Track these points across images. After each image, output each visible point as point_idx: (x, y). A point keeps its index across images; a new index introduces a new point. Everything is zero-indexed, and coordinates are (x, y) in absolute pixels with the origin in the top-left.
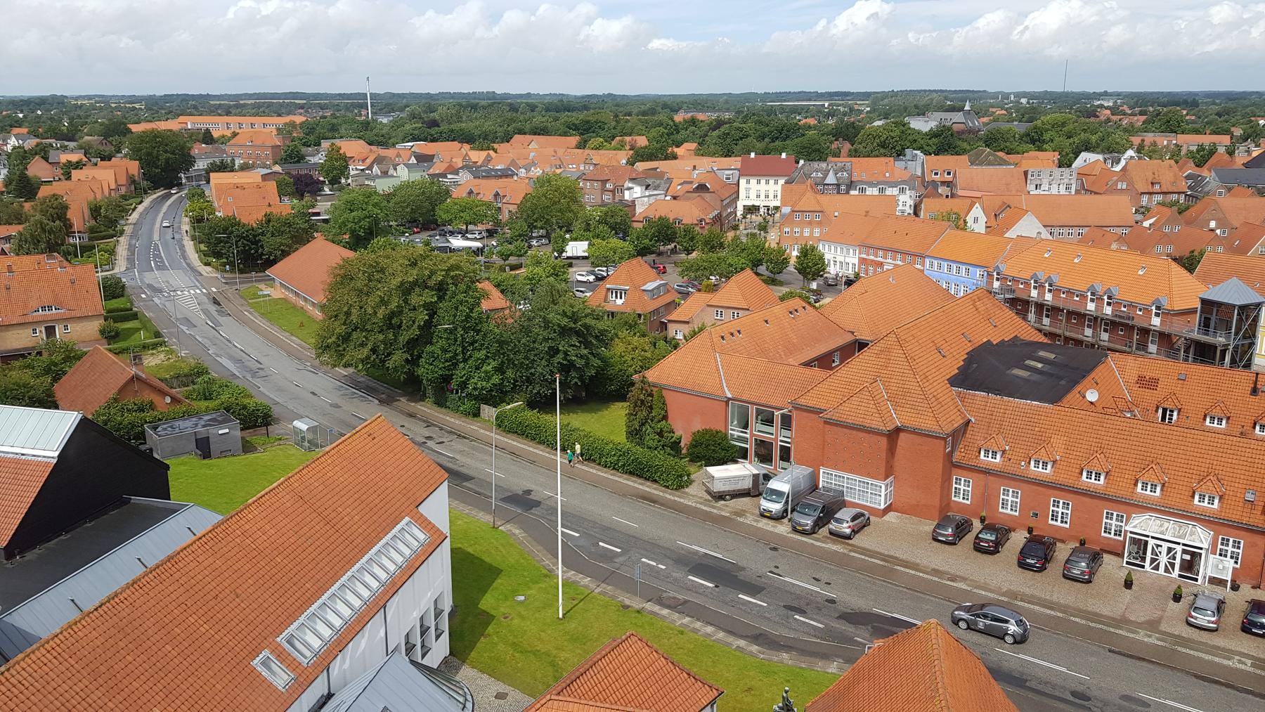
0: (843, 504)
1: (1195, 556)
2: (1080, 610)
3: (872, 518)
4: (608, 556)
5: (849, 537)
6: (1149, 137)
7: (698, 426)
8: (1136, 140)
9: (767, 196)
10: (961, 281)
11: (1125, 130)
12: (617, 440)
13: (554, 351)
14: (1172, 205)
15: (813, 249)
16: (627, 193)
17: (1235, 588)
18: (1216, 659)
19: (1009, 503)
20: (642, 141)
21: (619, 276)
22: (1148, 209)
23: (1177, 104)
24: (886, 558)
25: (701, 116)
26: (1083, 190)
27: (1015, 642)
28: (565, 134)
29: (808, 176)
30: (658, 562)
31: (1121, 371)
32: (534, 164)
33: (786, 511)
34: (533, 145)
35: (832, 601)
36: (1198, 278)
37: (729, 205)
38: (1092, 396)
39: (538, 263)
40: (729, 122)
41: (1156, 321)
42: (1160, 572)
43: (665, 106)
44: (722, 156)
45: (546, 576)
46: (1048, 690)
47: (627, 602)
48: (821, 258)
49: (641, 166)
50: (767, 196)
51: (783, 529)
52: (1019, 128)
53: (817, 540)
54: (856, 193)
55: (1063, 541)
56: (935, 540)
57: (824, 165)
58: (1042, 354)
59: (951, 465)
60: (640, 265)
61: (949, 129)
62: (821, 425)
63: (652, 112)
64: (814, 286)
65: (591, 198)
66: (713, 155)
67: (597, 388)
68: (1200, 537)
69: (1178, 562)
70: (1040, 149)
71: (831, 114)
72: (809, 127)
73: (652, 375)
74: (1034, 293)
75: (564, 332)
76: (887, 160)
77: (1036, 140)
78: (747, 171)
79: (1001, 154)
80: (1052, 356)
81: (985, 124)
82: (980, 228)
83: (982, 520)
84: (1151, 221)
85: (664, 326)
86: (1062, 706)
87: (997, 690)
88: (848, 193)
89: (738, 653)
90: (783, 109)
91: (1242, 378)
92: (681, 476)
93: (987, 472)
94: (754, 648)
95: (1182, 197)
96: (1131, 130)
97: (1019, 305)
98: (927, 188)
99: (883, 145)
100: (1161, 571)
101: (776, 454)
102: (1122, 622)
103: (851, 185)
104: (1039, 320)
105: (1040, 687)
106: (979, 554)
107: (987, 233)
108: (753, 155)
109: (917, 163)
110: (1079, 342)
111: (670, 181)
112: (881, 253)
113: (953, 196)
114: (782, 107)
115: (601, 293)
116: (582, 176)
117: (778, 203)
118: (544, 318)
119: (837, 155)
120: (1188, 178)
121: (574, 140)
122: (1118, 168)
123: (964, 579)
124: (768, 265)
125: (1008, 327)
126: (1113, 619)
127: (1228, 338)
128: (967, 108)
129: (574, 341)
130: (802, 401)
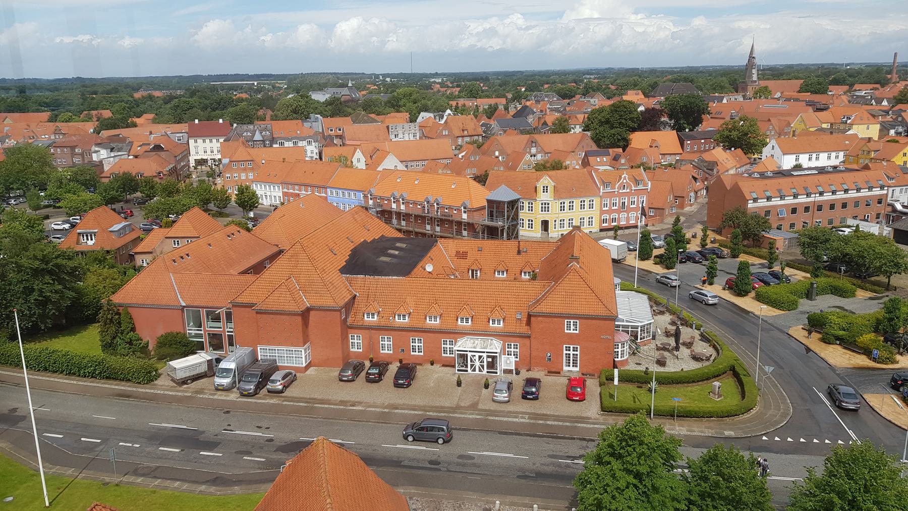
0: (277, 369)
1: (494, 358)
2: (432, 407)
3: (298, 375)
4: (91, 447)
5: (281, 392)
6: (461, 102)
7: (161, 331)
8: (454, 103)
9: (212, 152)
10: (346, 200)
11: (448, 97)
12: (92, 353)
13: (29, 291)
14: (475, 142)
15: (247, 188)
16: (94, 155)
17: (518, 373)
18: (510, 419)
19: (386, 346)
20: (107, 114)
21: (90, 222)
22: (461, 146)
23: (476, 80)
24: (307, 400)
25: (157, 94)
26: (424, 136)
27: (445, 442)
28: (38, 111)
29: (241, 135)
30: (133, 442)
31: (447, 250)
32: (8, 136)
33: (235, 382)
34: (8, 121)
35: (271, 440)
36: (487, 189)
37: (182, 160)
38: (429, 268)
39: (15, 218)
40: (180, 96)
41: (465, 216)
42: (477, 371)
43: (127, 86)
44: (175, 123)
45: (33, 475)
46: (414, 464)
47: (107, 479)
48: (254, 194)
49: (105, 134)
50: (212, 152)
51: (233, 396)
52: (383, 97)
53: (260, 398)
54: (278, 146)
55: (421, 364)
56: (341, 380)
57: (251, 127)
58: (398, 245)
59: (346, 328)
60: (105, 212)
61: (339, 99)
62: (255, 315)
63: (116, 90)
64: (252, 215)
65: (62, 163)
66: (167, 122)
67: (76, 315)
68: (496, 346)
69: (485, 364)
70: (398, 111)
71: (259, 91)
72: (242, 100)
73: (117, 298)
74: (394, 206)
75: (37, 273)
76: (297, 121)
77: (395, 105)
78: (195, 133)
79: (373, 116)
80: (404, 246)
81: (364, 95)
82: (362, 165)
83: (371, 361)
84: (463, 154)
85: (132, 257)
86: (420, 472)
87: (370, 473)
88: (271, 146)
89: (200, 496)
90: (223, 87)
91: (513, 244)
92: (150, 372)
93: (369, 328)
94: (213, 489)
95: (481, 138)
96: (451, 97)
97: (385, 215)
98: (326, 140)
99: (295, 111)
100: (477, 371)
101: (226, 341)
102: (457, 408)
103: (273, 141)
104: (399, 223)
105: (410, 464)
106: (369, 384)
107: (367, 169)
108: (197, 121)
109: (318, 123)
110: (424, 235)
111: (131, 143)
112: (297, 187)
113: (344, 145)
114: (222, 86)
115: (73, 237)
116: (53, 145)
117: (219, 157)
118: (16, 263)
119: (264, 119)
120: (482, 126)
121: (46, 115)
122: (442, 122)
123: (360, 403)
124: (212, 202)
125: (379, 230)
126: (451, 408)
127: (504, 222)
128: (350, 85)
129: (47, 279)
130: (239, 300)
